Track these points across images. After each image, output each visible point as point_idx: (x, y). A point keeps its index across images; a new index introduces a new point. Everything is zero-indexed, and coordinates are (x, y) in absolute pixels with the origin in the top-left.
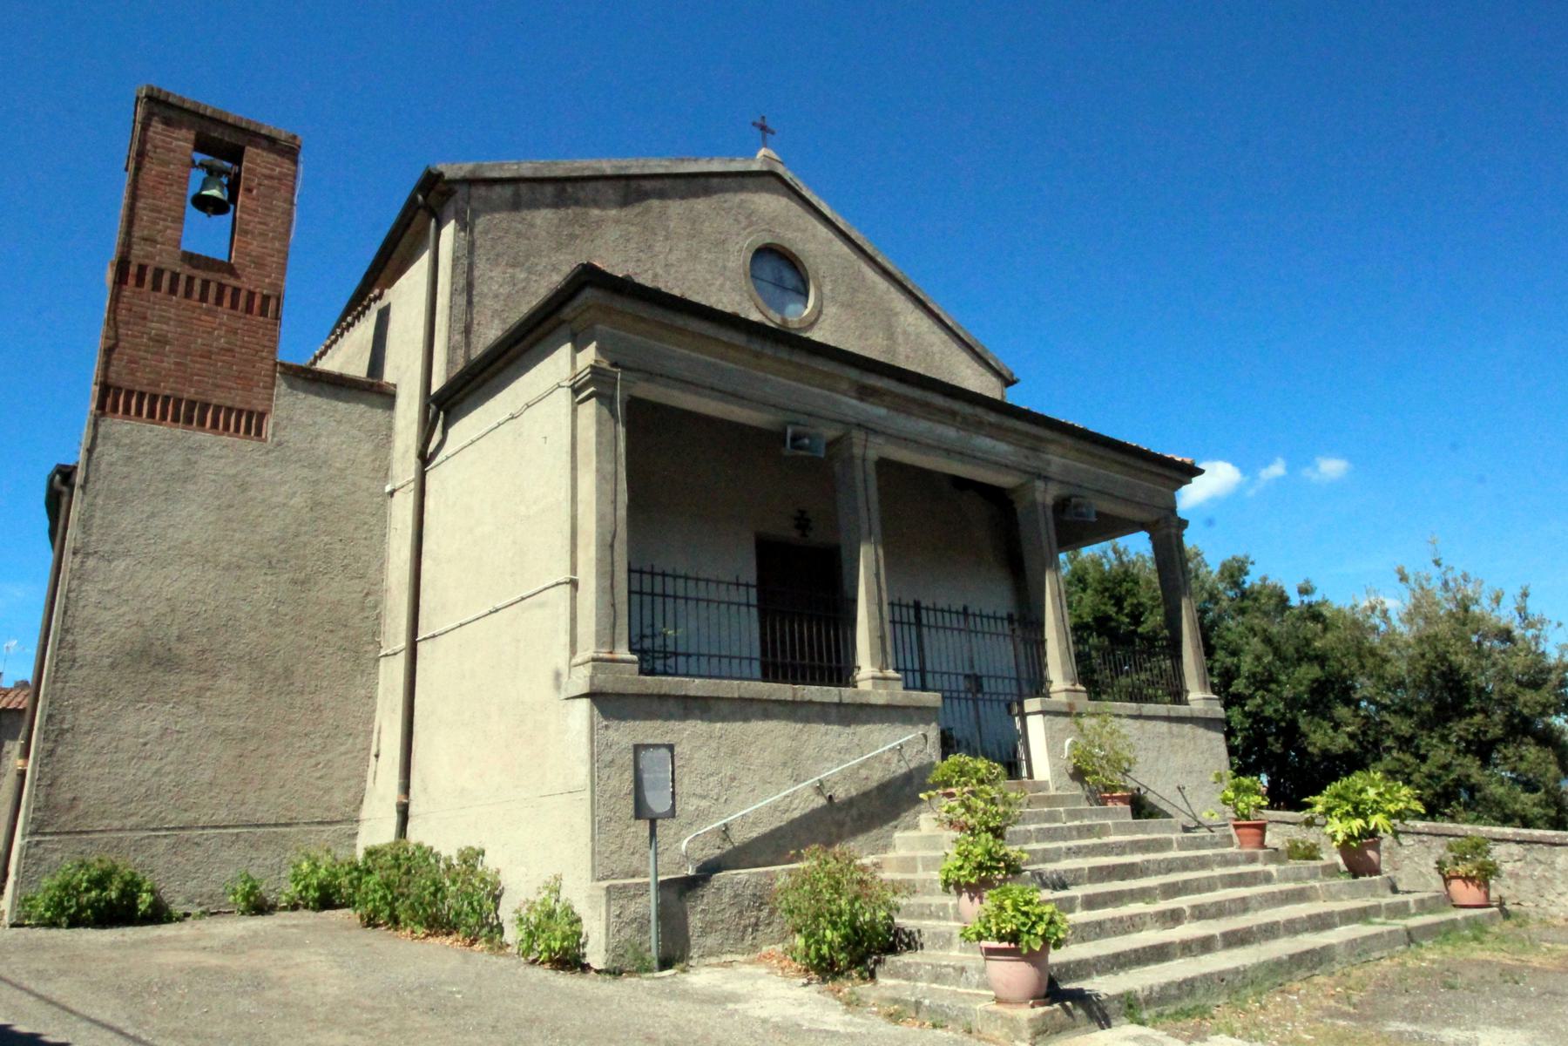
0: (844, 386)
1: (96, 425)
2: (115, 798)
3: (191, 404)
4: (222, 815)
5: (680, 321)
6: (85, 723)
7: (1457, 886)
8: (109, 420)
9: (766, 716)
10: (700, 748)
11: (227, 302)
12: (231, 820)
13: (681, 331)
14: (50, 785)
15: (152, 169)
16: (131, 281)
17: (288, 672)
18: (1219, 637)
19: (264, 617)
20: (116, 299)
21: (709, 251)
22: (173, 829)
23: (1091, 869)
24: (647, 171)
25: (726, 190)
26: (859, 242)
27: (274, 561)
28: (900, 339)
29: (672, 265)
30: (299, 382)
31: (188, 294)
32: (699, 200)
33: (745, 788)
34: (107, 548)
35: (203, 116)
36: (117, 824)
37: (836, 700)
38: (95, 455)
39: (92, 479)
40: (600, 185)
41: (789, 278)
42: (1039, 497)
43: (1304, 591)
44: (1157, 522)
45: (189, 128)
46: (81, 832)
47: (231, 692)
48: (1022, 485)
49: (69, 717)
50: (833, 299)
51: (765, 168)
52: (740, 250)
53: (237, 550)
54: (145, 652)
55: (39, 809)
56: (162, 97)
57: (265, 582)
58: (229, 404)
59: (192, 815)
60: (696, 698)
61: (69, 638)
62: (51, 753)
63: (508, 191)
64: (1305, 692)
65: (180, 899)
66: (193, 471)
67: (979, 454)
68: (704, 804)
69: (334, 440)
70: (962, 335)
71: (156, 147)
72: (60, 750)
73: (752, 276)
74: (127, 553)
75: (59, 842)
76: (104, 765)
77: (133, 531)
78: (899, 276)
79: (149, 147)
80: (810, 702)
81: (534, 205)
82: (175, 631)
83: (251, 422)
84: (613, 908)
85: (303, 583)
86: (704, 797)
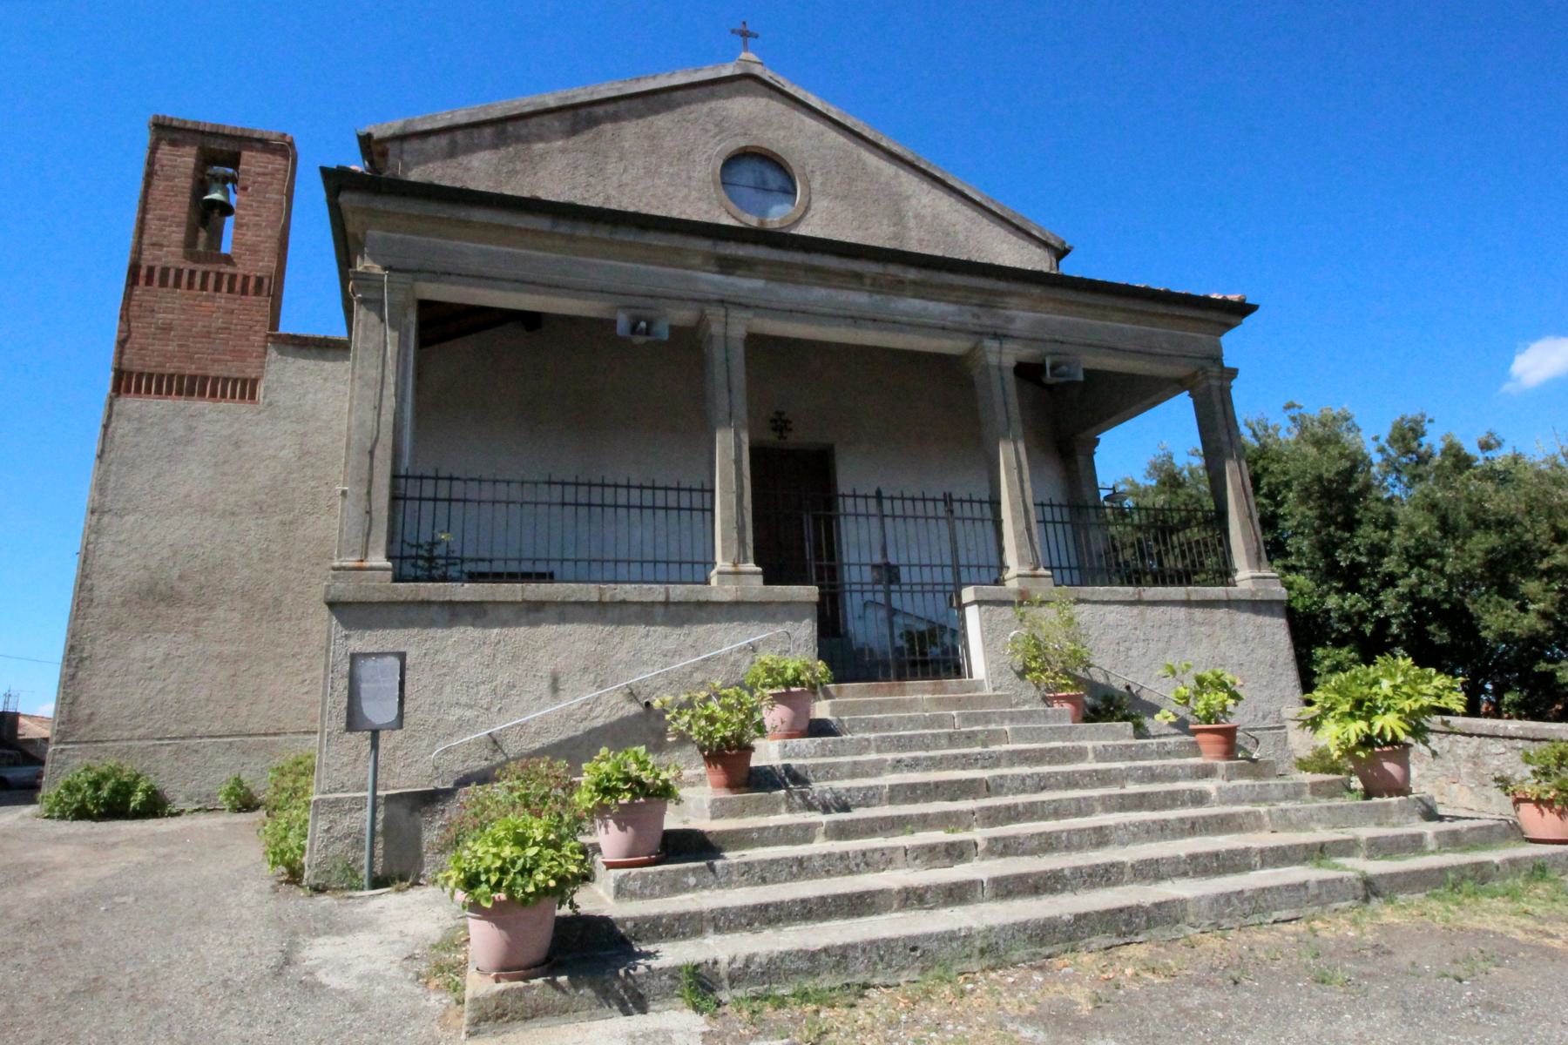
0: (698, 261)
1: (111, 406)
2: (126, 713)
3: (193, 378)
4: (217, 727)
5: (462, 213)
6: (100, 651)
7: (1528, 812)
8: (122, 400)
9: (562, 619)
10: (470, 654)
11: (225, 288)
12: (224, 730)
13: (466, 223)
14: (72, 703)
15: (159, 185)
16: (142, 282)
17: (277, 602)
18: (1366, 509)
19: (256, 556)
20: (128, 297)
21: (671, 164)
22: (175, 738)
23: (893, 788)
24: (596, 97)
25: (689, 103)
26: (857, 129)
27: (264, 508)
28: (912, 223)
29: (627, 184)
30: (290, 348)
31: (190, 285)
32: (659, 117)
33: (527, 697)
34: (120, 505)
35: (203, 133)
36: (126, 734)
37: (661, 598)
38: (110, 430)
39: (107, 450)
40: (546, 119)
41: (773, 178)
42: (993, 359)
43: (1485, 446)
44: (1194, 375)
45: (192, 145)
46: (96, 742)
47: (225, 621)
48: (973, 349)
49: (88, 647)
50: (824, 193)
51: (738, 72)
52: (709, 158)
53: (232, 499)
54: (150, 591)
55: (63, 723)
56: (167, 123)
57: (257, 525)
58: (225, 374)
59: (192, 726)
60: (458, 603)
61: (88, 582)
62: (73, 677)
63: (443, 141)
64: (1479, 566)
65: (181, 797)
66: (193, 436)
67: (898, 318)
68: (469, 713)
69: (320, 396)
70: (993, 208)
71: (162, 166)
72: (80, 674)
73: (723, 183)
74: (135, 509)
75: (80, 749)
76: (116, 686)
77: (142, 489)
78: (909, 157)
79: (157, 167)
80: (623, 602)
81: (471, 149)
82: (176, 573)
83: (246, 389)
84: (319, 824)
85: (291, 523)
86: (471, 707)
